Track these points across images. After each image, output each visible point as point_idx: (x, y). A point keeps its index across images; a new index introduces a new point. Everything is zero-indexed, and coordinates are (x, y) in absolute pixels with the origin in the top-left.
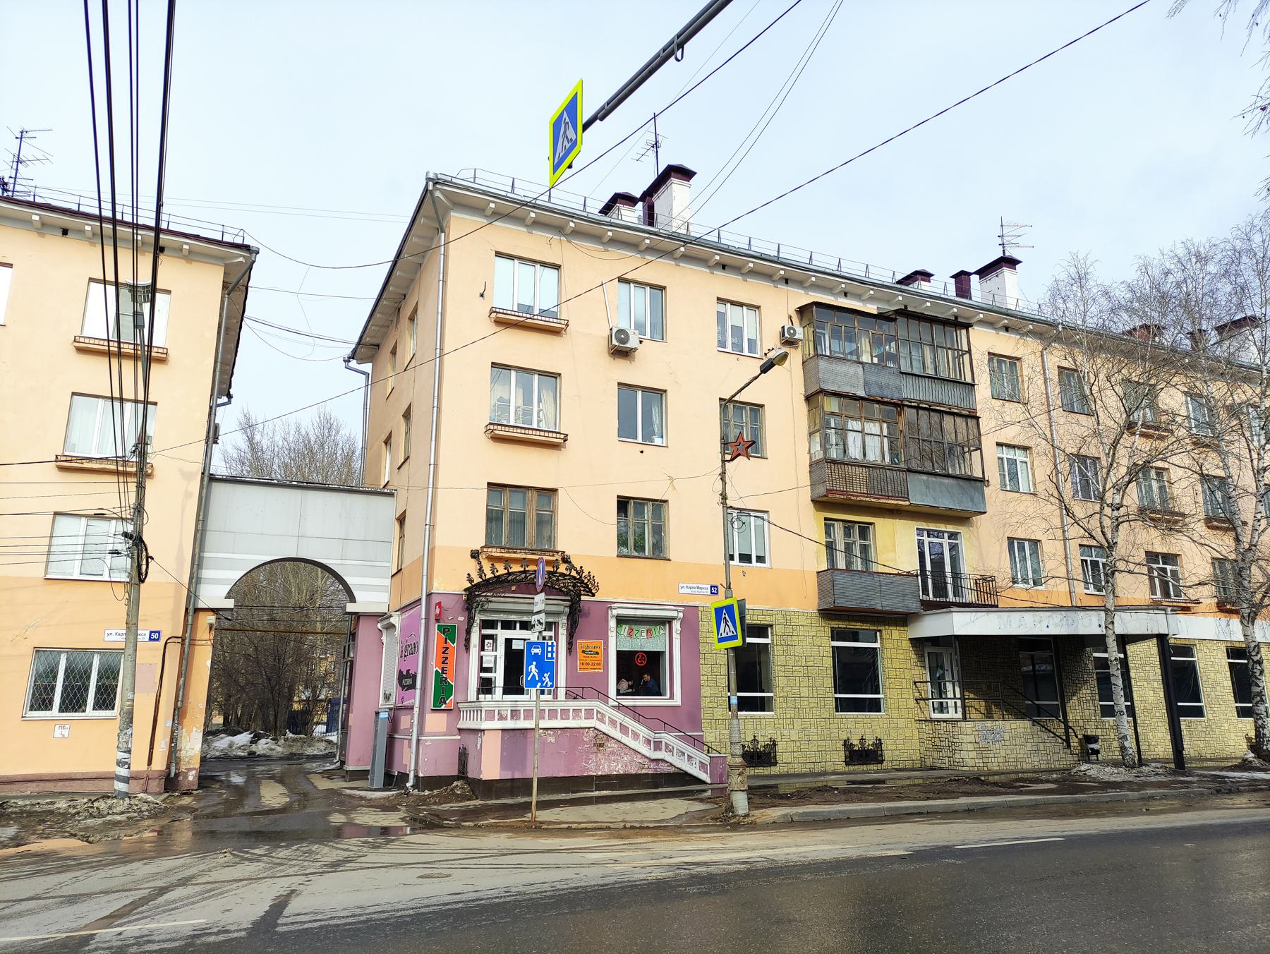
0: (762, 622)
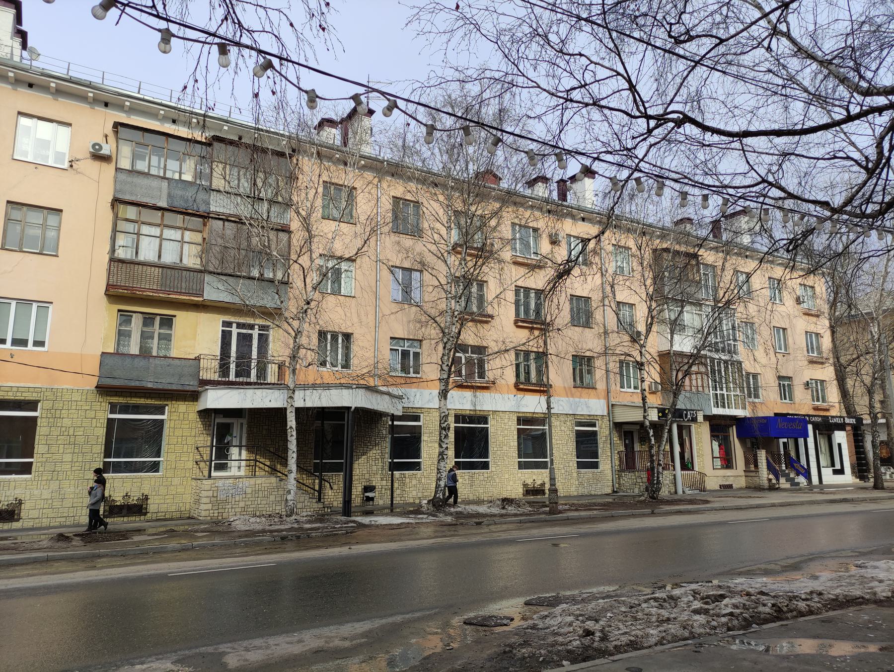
0: (27, 398)
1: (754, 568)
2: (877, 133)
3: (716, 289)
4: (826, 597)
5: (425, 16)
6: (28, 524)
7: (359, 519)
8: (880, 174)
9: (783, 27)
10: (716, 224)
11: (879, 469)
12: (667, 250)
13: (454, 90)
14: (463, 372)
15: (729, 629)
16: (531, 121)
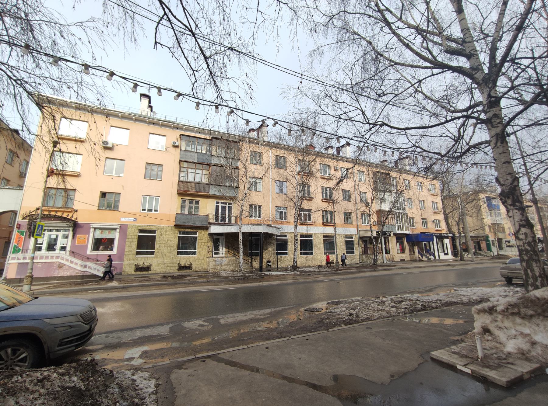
1: (414, 290)
2: (458, 127)
3: (397, 187)
4: (443, 302)
5: (287, 91)
6: (154, 272)
7: (265, 273)
8: (460, 142)
9: (419, 89)
10: (396, 162)
11: (462, 253)
12: (378, 172)
13: (298, 117)
14: (303, 219)
15: (405, 314)
16: (326, 126)
